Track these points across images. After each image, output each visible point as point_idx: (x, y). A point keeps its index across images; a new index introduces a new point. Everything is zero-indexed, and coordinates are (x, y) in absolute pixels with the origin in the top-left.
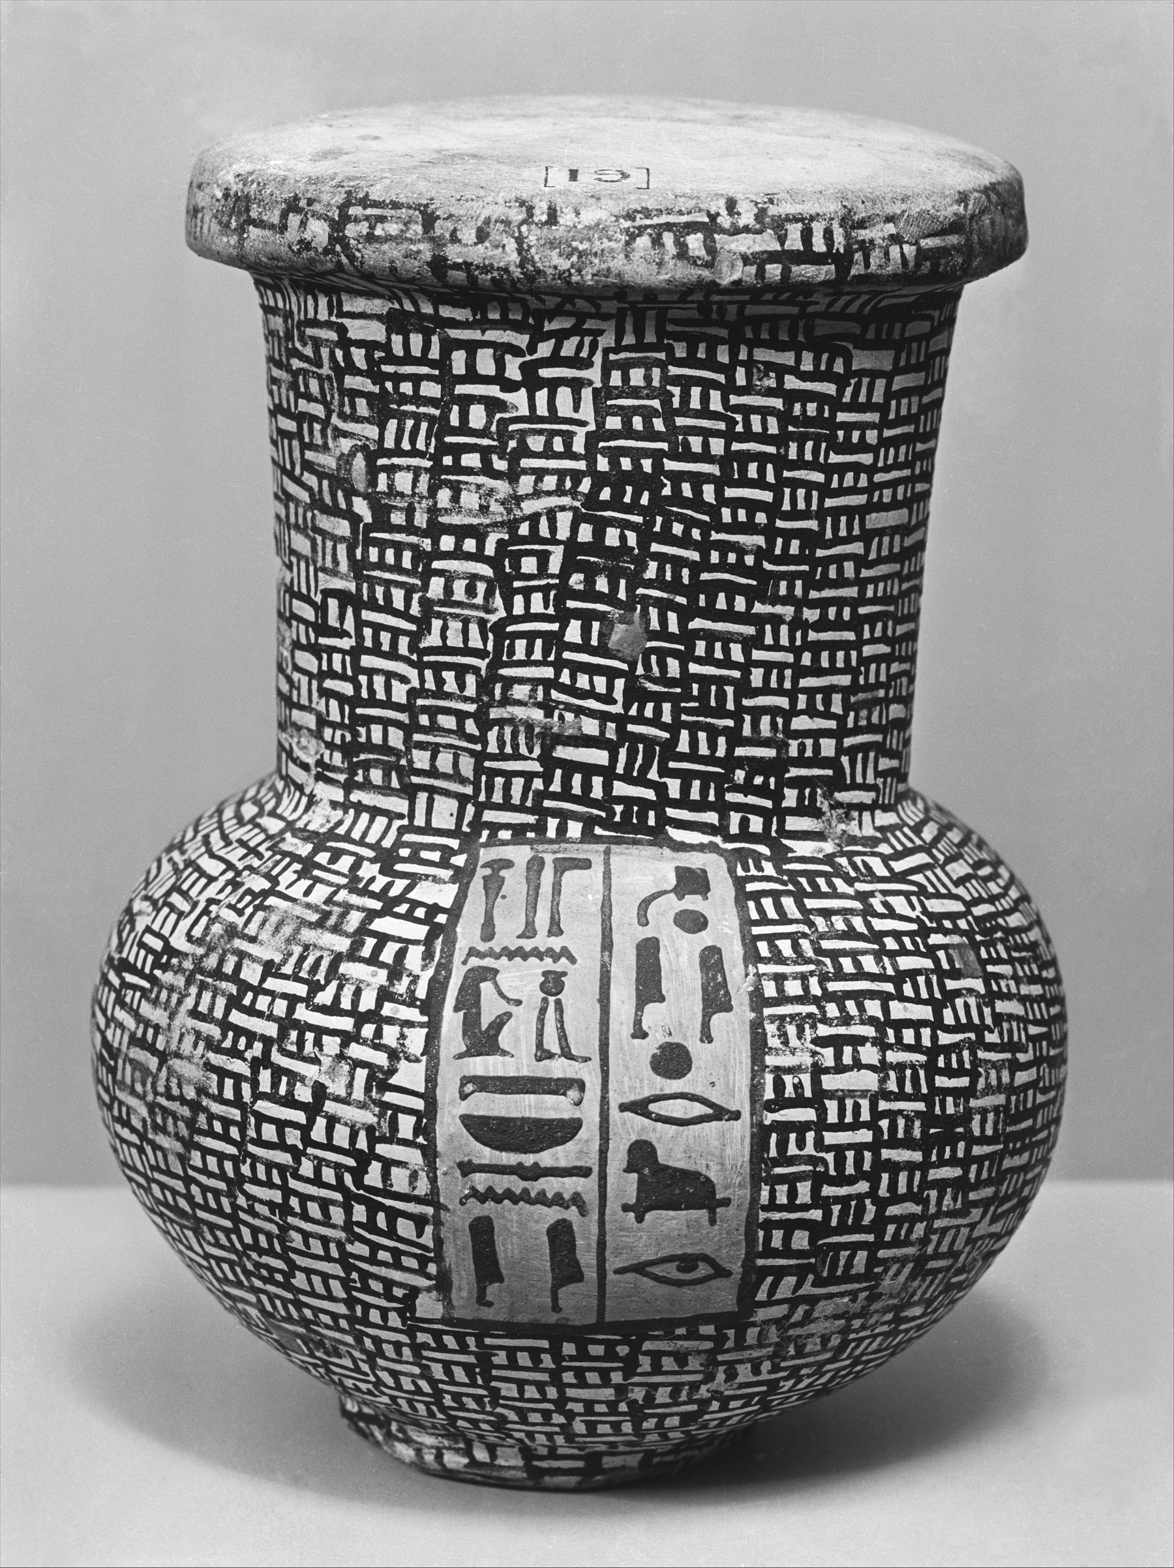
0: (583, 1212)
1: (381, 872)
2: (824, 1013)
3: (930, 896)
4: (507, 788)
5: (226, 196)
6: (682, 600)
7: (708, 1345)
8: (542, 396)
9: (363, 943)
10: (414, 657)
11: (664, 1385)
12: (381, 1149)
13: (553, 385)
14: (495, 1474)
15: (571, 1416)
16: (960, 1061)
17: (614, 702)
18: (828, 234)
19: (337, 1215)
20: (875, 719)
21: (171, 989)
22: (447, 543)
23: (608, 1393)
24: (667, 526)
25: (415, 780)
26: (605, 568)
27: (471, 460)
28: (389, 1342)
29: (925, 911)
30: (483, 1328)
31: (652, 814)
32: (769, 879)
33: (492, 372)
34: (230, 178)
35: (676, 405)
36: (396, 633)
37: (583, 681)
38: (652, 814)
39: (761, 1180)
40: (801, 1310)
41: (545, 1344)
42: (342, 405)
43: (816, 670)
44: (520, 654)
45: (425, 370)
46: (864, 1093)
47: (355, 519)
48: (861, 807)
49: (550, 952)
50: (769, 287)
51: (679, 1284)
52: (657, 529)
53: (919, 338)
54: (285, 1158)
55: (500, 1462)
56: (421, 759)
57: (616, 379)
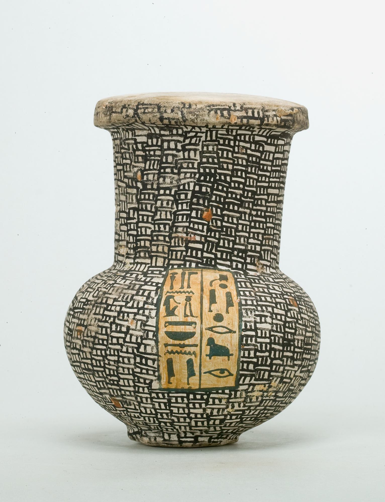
0: (196, 356)
1: (144, 276)
2: (257, 309)
3: (284, 288)
4: (176, 256)
5: (106, 107)
6: (221, 206)
7: (227, 396)
8: (186, 154)
9: (139, 292)
10: (153, 222)
11: (216, 408)
12: (144, 341)
13: (189, 150)
14: (170, 443)
15: (191, 419)
16: (292, 326)
17: (204, 232)
18: (258, 113)
19: (132, 361)
20: (270, 244)
21: (88, 309)
22: (162, 192)
23: (201, 411)
24: (218, 187)
25: (152, 254)
26: (202, 197)
27: (168, 170)
28: (144, 397)
29: (283, 290)
30: (169, 391)
31: (213, 261)
32: (243, 279)
33: (174, 148)
34: (107, 103)
35: (220, 156)
36: (148, 216)
37: (196, 226)
38: (213, 261)
39: (241, 349)
40: (251, 387)
41: (185, 395)
42: (135, 159)
43: (255, 227)
44: (180, 219)
45: (157, 148)
46: (267, 329)
47: (137, 188)
48: (267, 266)
49: (188, 292)
50: (243, 125)
51: (220, 377)
52: (215, 187)
53: (282, 145)
54: (118, 347)
55: (171, 439)
56: (154, 248)
57: (205, 149)
